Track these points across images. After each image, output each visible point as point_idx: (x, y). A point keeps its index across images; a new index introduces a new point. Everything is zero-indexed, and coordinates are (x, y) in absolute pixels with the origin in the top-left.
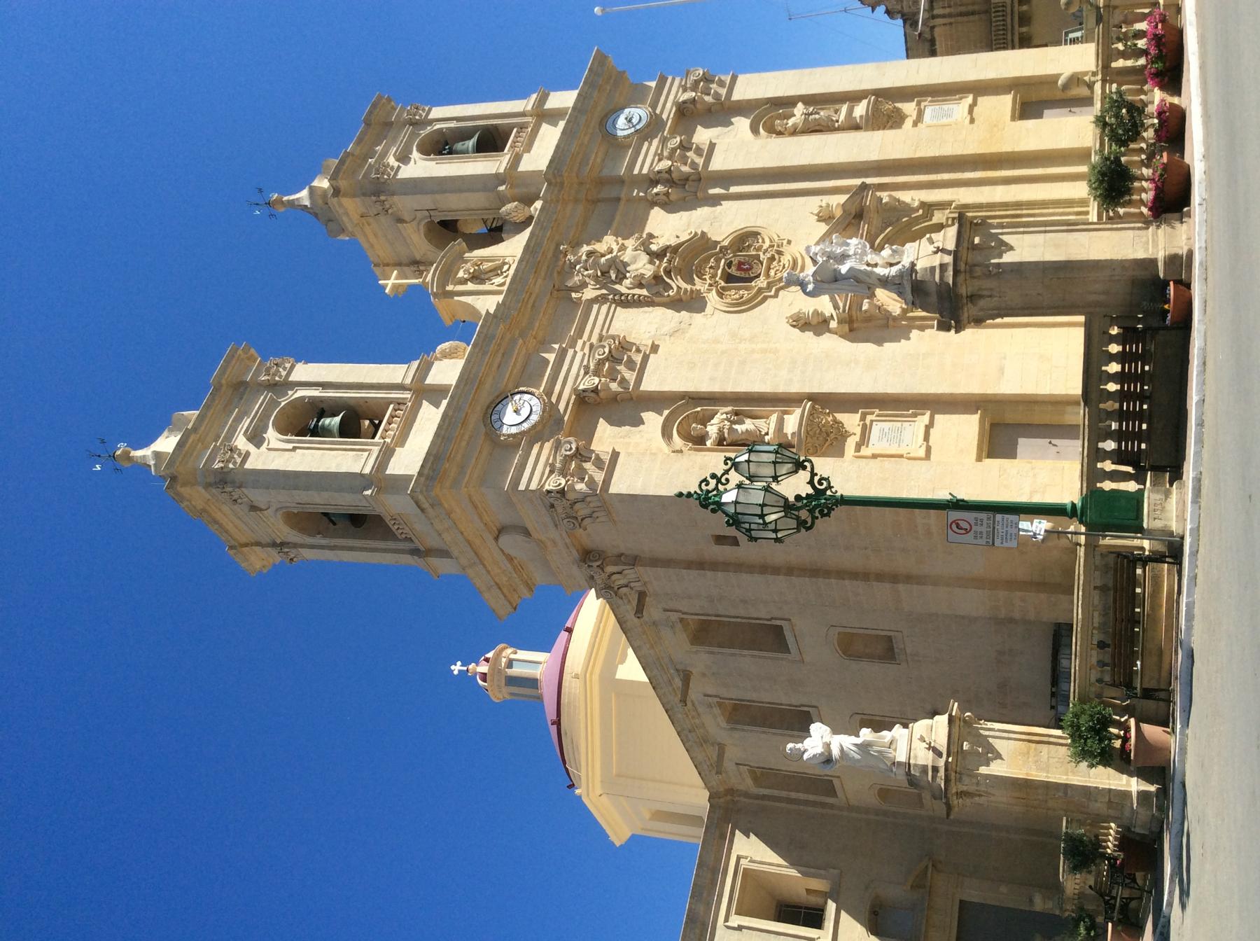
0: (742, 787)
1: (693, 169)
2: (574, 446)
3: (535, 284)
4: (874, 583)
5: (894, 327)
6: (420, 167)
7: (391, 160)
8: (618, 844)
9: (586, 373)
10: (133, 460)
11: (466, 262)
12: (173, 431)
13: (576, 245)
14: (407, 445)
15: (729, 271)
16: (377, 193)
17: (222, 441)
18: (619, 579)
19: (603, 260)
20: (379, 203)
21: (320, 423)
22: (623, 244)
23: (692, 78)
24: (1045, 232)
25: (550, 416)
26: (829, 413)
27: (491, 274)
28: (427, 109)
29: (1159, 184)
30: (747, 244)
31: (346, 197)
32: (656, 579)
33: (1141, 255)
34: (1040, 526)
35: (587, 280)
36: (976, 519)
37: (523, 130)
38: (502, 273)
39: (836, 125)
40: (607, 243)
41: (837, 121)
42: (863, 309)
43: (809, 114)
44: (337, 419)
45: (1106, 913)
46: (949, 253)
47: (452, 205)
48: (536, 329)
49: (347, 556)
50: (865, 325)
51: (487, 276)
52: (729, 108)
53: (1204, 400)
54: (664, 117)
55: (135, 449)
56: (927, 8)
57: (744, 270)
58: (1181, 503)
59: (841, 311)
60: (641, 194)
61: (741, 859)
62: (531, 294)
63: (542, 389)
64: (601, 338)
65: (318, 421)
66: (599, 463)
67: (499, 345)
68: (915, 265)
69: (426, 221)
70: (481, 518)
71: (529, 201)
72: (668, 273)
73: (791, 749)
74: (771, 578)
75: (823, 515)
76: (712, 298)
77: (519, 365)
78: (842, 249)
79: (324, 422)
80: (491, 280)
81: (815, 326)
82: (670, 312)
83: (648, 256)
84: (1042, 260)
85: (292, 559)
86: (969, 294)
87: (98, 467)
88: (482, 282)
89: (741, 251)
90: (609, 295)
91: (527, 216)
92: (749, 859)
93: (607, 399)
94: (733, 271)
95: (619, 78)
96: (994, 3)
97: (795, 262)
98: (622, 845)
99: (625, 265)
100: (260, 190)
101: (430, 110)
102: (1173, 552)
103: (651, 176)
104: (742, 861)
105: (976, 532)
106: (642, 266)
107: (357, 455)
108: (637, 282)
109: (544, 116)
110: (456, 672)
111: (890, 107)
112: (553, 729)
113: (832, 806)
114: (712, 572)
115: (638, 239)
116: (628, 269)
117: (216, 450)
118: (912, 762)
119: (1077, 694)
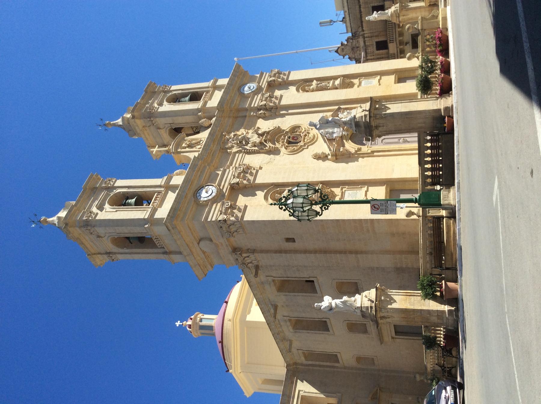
0: (299, 361)
1: (274, 104)
2: (229, 204)
3: (213, 147)
4: (349, 255)
5: (352, 157)
6: (167, 107)
7: (156, 105)
8: (248, 396)
9: (234, 178)
10: (48, 222)
11: (186, 141)
12: (65, 209)
13: (229, 133)
14: (163, 207)
15: (289, 140)
16: (150, 118)
17: (87, 210)
18: (248, 260)
19: (240, 137)
20: (150, 121)
21: (127, 202)
22: (248, 132)
23: (273, 73)
24: (402, 103)
25: (220, 194)
26: (329, 188)
27: (196, 145)
28: (170, 86)
29: (441, 84)
30: (296, 130)
31: (137, 119)
32: (263, 260)
33: (435, 108)
34: (404, 205)
35: (234, 145)
36: (381, 204)
37: (208, 93)
38: (200, 144)
39: (329, 88)
40: (241, 132)
41: (329, 86)
42: (341, 151)
43: (318, 84)
44: (134, 200)
45: (443, 373)
46: (367, 111)
47: (180, 121)
48: (214, 163)
49: (136, 257)
50: (342, 157)
51: (194, 145)
52: (288, 84)
53: (459, 154)
54: (263, 86)
55: (49, 218)
56: (364, 56)
57: (295, 139)
58: (454, 194)
59: (332, 151)
60: (254, 114)
61: (300, 392)
62: (212, 150)
63: (216, 184)
64: (240, 165)
65: (126, 201)
66: (239, 209)
67: (200, 168)
68: (356, 116)
69: (169, 128)
70: (192, 234)
71: (211, 119)
72: (265, 141)
73: (316, 305)
74: (308, 255)
75: (325, 209)
76: (283, 150)
77: (207, 175)
78: (332, 130)
79: (128, 201)
80: (196, 147)
81: (323, 158)
82: (266, 155)
83: (258, 135)
84: (400, 111)
85: (113, 260)
86: (375, 126)
87: (33, 226)
88: (192, 147)
89: (294, 133)
90: (242, 150)
91: (210, 124)
92: (304, 391)
93: (242, 187)
94: (291, 140)
95: (245, 73)
96: (391, 54)
97: (314, 136)
98: (249, 397)
99: (249, 139)
100: (102, 120)
101: (171, 87)
102: (452, 215)
103: (259, 107)
104: (301, 392)
105: (381, 209)
106: (255, 139)
107: (143, 212)
108: (253, 145)
109: (216, 87)
110: (178, 325)
111: (349, 81)
112: (219, 345)
113: (337, 367)
114: (285, 254)
115: (253, 129)
116: (250, 140)
117: (84, 213)
118: (363, 306)
119: (422, 273)
